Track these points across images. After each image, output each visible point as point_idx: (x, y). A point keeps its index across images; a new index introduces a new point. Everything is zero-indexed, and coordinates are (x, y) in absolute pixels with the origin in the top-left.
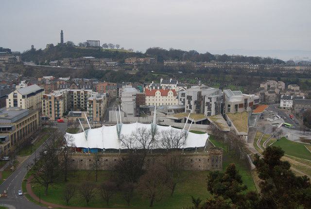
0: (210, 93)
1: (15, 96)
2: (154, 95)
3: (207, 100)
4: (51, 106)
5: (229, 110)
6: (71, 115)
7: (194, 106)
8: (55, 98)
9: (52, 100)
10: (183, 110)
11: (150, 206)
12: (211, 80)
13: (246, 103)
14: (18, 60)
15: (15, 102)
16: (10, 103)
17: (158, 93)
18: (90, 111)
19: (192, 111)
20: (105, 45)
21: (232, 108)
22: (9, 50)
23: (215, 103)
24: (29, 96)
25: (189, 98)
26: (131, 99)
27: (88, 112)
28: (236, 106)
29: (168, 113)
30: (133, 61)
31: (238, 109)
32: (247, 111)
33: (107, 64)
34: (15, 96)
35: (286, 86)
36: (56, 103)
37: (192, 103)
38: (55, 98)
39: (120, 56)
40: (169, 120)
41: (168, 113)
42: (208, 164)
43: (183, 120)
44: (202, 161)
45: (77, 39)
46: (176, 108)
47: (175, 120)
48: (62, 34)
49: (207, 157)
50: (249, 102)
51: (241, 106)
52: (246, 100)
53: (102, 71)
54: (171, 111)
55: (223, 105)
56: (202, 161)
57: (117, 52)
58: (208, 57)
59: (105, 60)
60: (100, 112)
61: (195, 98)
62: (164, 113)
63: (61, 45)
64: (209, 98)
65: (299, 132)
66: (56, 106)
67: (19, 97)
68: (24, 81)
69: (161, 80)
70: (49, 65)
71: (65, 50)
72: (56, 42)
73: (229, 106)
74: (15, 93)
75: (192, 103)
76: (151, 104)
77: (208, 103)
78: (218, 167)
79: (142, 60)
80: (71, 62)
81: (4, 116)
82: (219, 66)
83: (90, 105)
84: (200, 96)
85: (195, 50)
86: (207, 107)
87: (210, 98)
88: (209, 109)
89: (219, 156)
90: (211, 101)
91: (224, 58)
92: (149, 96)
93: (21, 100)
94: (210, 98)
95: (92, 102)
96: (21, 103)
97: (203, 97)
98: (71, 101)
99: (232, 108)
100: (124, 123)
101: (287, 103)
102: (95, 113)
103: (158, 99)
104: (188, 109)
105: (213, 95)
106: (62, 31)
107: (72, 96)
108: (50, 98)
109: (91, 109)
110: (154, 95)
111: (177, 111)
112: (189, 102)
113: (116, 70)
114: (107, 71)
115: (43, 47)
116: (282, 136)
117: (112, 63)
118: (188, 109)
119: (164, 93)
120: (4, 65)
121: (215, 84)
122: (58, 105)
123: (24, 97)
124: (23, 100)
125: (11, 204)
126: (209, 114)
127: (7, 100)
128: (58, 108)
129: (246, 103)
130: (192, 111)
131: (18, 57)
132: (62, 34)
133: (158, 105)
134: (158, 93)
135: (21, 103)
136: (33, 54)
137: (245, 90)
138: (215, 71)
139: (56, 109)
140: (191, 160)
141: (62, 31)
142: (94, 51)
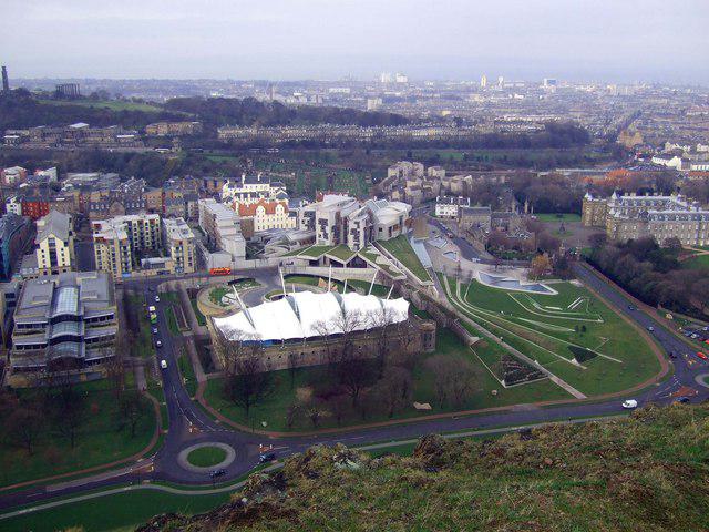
1: (52, 245)
3: (352, 226)
6: (148, 266)
7: (331, 235)
9: (117, 246)
26: (234, 231)
33: (116, 139)
34: (52, 245)
44: (289, 284)
55: (372, 228)
61: (332, 222)
68: (14, 199)
73: (381, 230)
75: (328, 229)
77: (353, 231)
81: (96, 297)
82: (311, 134)
88: (357, 238)
101: (445, 210)
102: (186, 260)
106: (4, 68)
108: (112, 242)
112: (323, 229)
125: (223, 442)
141: (4, 68)
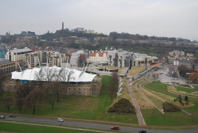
0: (123, 54)
1: (10, 53)
2: (95, 56)
3: (119, 58)
4: (29, 59)
5: (135, 65)
7: (113, 62)
8: (32, 55)
9: (30, 56)
10: (107, 64)
11: (33, 113)
12: (141, 50)
13: (146, 61)
14: (37, 38)
15: (10, 56)
16: (7, 57)
17: (97, 54)
18: (51, 63)
19: (112, 65)
20: (86, 30)
21: (137, 64)
22: (34, 33)
23: (124, 60)
24: (18, 54)
25: (110, 57)
26: (76, 57)
27: (50, 63)
28: (139, 62)
29: (98, 66)
30: (99, 38)
31: (141, 64)
32: (147, 65)
34: (10, 53)
35: (185, 54)
36: (32, 58)
37: (112, 60)
38: (32, 55)
39: (91, 36)
40: (96, 69)
41: (98, 66)
42: (90, 92)
43: (104, 70)
44: (86, 90)
45: (71, 26)
46: (103, 63)
47: (99, 69)
48: (63, 24)
49: (89, 88)
50: (148, 60)
51: (143, 62)
52: (146, 59)
53: (78, 44)
54: (100, 64)
56: (86, 90)
57: (91, 34)
58: (146, 37)
59: (82, 38)
60: (57, 63)
61: (113, 57)
62: (96, 66)
63: (63, 30)
64: (121, 57)
65: (172, 78)
66: (32, 59)
67: (12, 54)
69: (106, 48)
70: (52, 40)
71: (64, 33)
72: (60, 28)
73: (135, 62)
74: (10, 52)
75: (112, 60)
76: (93, 61)
77: (120, 60)
78: (96, 94)
79: (103, 38)
80: (64, 39)
83: (51, 60)
84: (117, 56)
85: (139, 34)
86: (120, 62)
87: (121, 57)
88: (121, 63)
89: (96, 87)
90: (122, 59)
91: (153, 38)
92: (92, 56)
93: (13, 56)
94: (121, 57)
95: (52, 57)
96: (13, 57)
97: (69, 52)
98: (45, 58)
99: (137, 64)
100: (86, 72)
103: (97, 58)
104: (110, 63)
105: (124, 55)
106: (63, 23)
107: (46, 55)
109: (52, 62)
110: (95, 56)
111: (104, 65)
113: (86, 44)
114: (81, 44)
115: (54, 32)
116: (158, 80)
117: (86, 40)
118: (110, 63)
119: (101, 55)
120: (29, 41)
121: (142, 52)
122: (33, 59)
123: (15, 54)
124: (14, 56)
126: (121, 66)
127: (6, 55)
128: (33, 61)
129: (146, 61)
130: (112, 65)
131: (37, 37)
132: (63, 24)
133: (97, 61)
134: (97, 54)
135: (13, 57)
136: (48, 36)
137: (159, 56)
138: (144, 45)
139: (32, 61)
140: (80, 89)
141: (63, 23)
142: (80, 34)
